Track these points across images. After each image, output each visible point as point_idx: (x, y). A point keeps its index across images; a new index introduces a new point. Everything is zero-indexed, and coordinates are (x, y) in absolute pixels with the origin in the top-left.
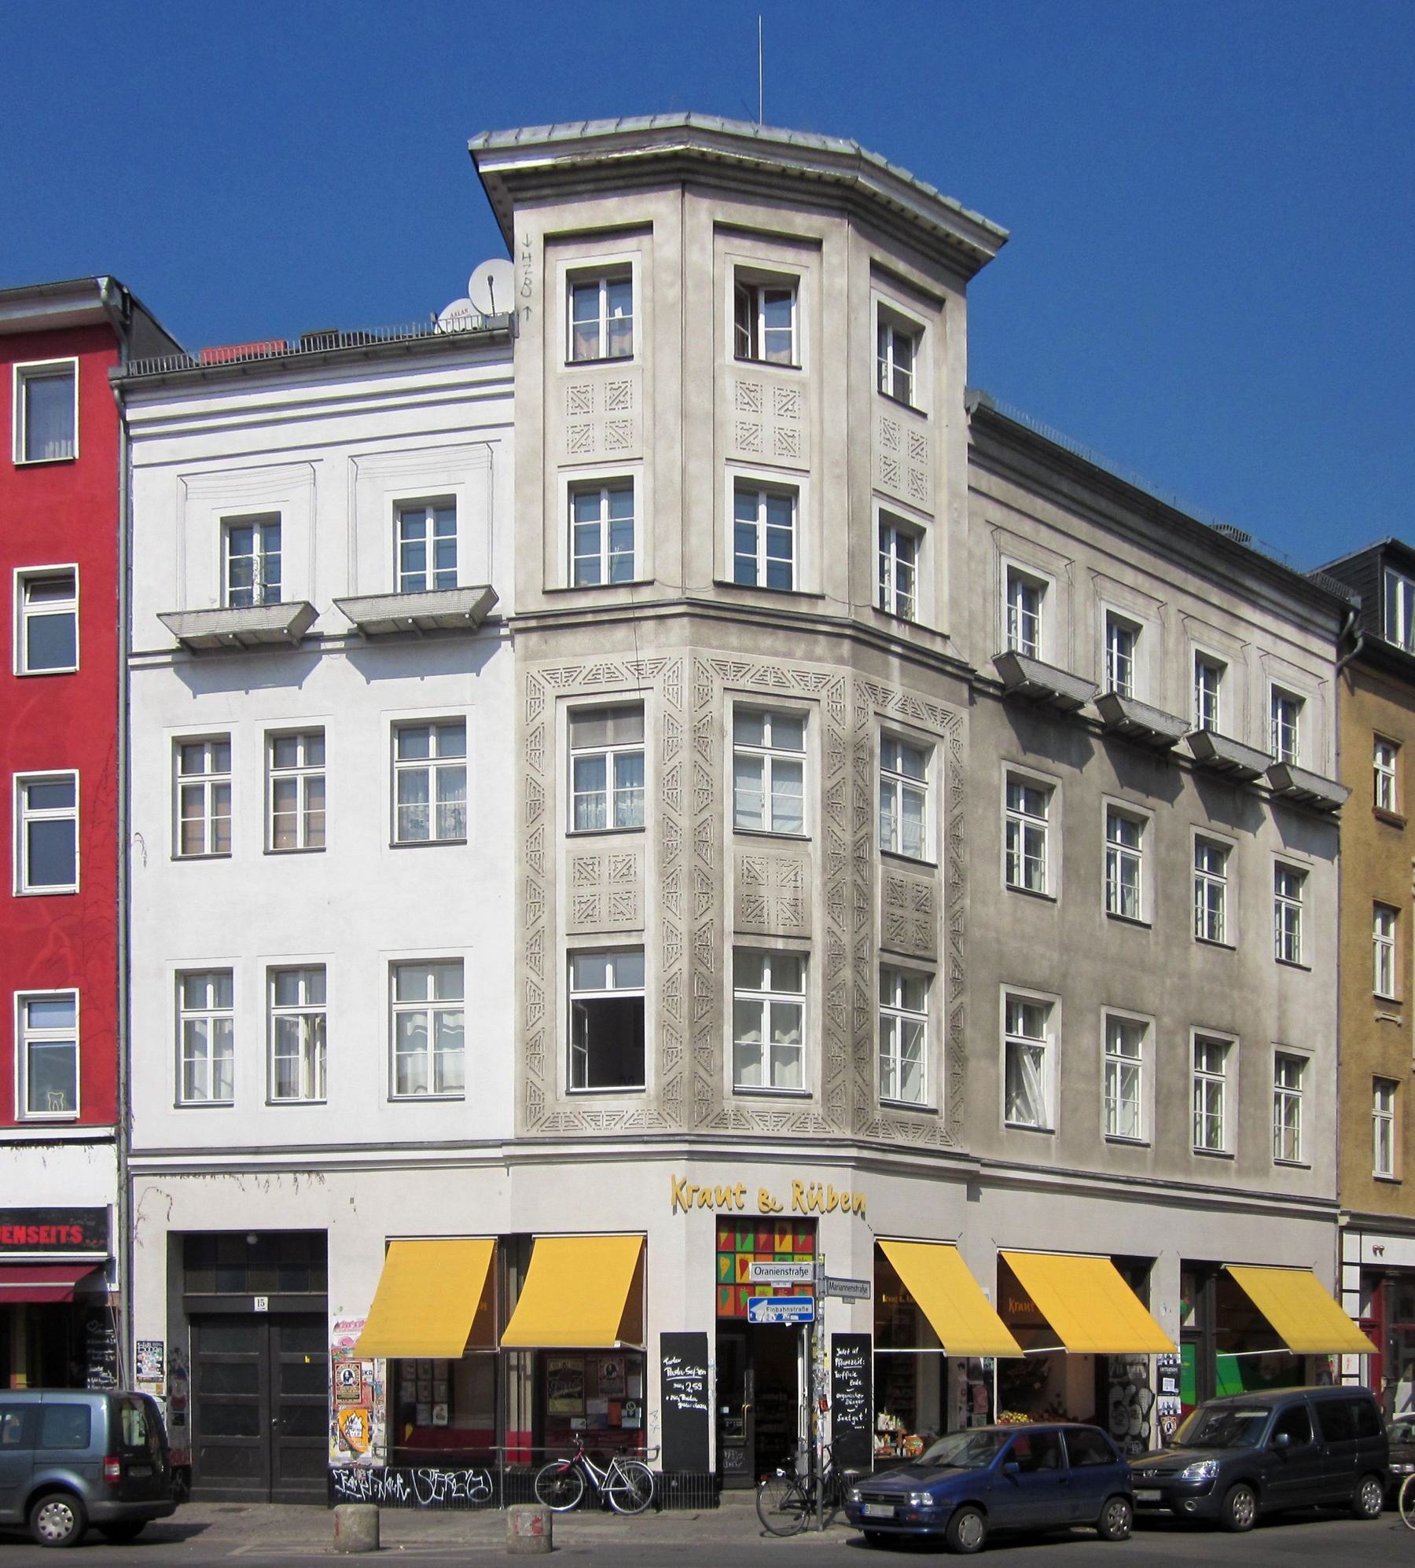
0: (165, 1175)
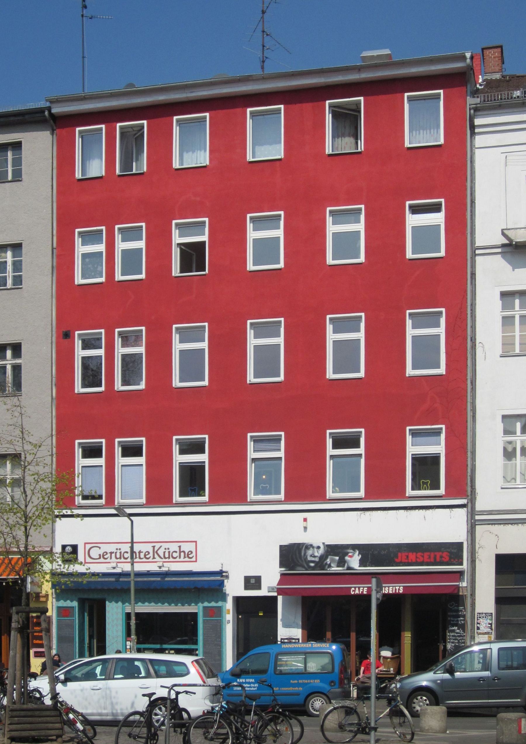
0: (495, 524)
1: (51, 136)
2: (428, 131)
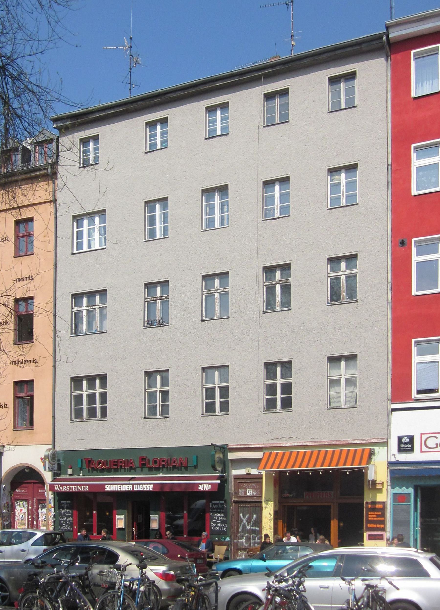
1: (386, 62)
2: (431, 82)
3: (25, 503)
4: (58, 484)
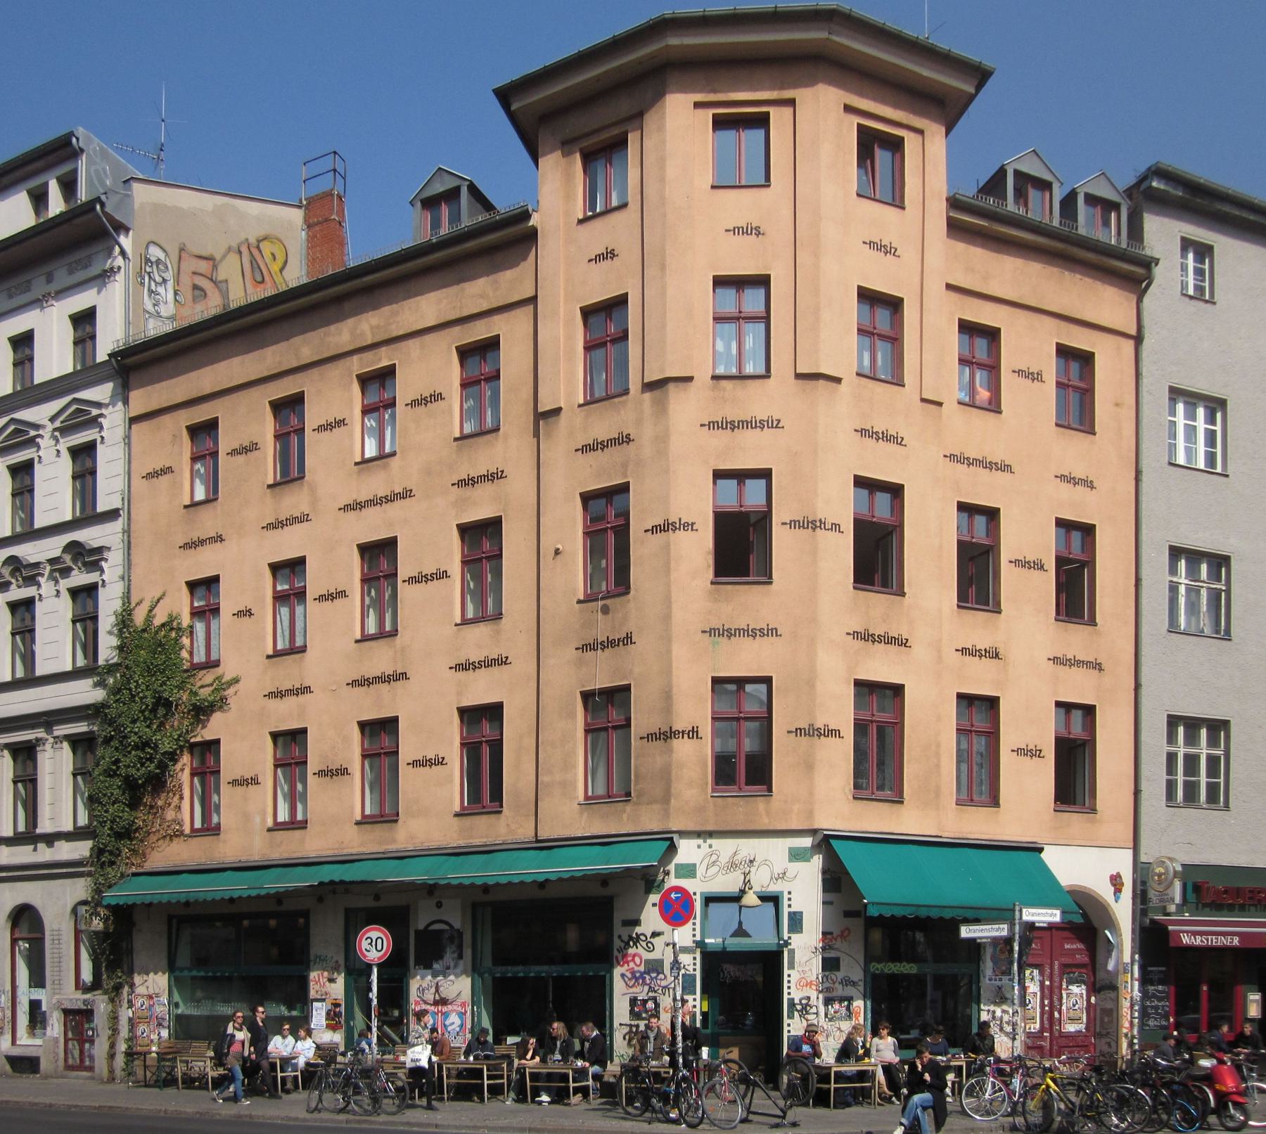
3: (1036, 972)
4: (1187, 932)
